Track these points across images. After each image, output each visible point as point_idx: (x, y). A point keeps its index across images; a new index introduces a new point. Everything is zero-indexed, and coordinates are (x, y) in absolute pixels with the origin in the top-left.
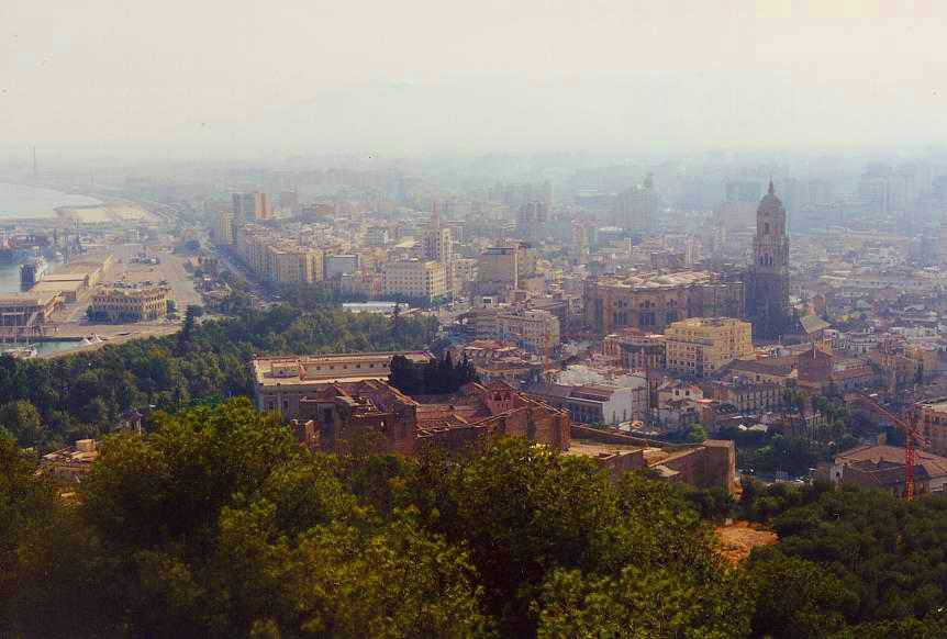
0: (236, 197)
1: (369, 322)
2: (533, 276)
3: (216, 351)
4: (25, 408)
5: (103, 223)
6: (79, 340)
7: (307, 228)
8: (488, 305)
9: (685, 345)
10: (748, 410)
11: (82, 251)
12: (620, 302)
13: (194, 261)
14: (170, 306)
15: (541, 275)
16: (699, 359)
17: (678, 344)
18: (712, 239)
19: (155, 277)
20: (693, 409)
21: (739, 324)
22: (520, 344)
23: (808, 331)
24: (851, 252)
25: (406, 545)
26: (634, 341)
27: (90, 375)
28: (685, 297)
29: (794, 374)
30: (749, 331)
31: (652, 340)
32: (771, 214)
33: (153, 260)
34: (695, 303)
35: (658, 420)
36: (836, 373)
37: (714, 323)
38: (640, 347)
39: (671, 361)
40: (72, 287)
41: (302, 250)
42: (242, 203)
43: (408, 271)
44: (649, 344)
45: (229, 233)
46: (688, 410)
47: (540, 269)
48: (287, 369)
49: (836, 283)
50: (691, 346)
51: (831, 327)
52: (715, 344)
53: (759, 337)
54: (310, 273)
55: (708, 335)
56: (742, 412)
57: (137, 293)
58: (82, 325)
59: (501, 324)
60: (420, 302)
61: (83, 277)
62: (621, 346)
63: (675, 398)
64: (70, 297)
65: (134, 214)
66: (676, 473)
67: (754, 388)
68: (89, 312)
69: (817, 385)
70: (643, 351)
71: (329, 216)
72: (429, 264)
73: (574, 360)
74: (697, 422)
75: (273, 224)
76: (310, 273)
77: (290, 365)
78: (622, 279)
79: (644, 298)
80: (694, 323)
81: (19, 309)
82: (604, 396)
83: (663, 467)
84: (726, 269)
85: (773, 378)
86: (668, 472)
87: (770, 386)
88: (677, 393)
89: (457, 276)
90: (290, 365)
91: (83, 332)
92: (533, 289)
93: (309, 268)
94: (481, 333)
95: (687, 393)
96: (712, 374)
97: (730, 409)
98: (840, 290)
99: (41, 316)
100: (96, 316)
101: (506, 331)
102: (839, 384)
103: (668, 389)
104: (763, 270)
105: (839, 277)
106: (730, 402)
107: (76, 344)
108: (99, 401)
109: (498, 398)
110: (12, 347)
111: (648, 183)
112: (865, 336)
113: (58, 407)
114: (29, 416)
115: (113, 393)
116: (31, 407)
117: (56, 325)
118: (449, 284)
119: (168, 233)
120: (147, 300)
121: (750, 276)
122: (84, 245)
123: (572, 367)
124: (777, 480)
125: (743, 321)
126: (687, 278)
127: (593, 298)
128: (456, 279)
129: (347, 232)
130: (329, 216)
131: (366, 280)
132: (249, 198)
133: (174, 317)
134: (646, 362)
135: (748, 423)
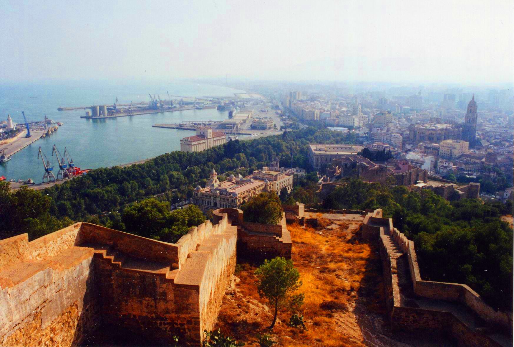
0: (291, 93)
1: (338, 134)
2: (391, 123)
3: (294, 140)
4: (242, 155)
5: (249, 99)
6: (250, 134)
7: (313, 103)
8: (378, 131)
9: (446, 148)
10: (468, 171)
11: (245, 107)
12: (422, 133)
13: (279, 112)
14: (275, 126)
15: (393, 122)
16: (451, 153)
17: (444, 148)
18: (441, 112)
19: (268, 116)
20: (451, 169)
21: (465, 142)
22: (390, 144)
23: (483, 145)
24: (490, 119)
25: (436, 222)
26: (429, 146)
27: (260, 146)
28: (443, 132)
29: (484, 160)
30: (468, 145)
31: (434, 146)
32: (472, 106)
33: (266, 111)
34: (446, 134)
35: (439, 172)
36: (498, 160)
37: (457, 142)
38: (431, 148)
39: (441, 153)
40: (245, 118)
41: (313, 110)
42: (293, 95)
43: (346, 118)
44: (434, 147)
45: (288, 103)
46: (450, 169)
47: (393, 121)
48: (321, 148)
49: (488, 129)
50: (449, 148)
51: (490, 145)
52: (457, 148)
53: (471, 146)
54: (316, 117)
55: (455, 146)
56: (467, 171)
57: (265, 121)
58: (248, 130)
59: (384, 137)
60: (350, 128)
61: (247, 115)
62: (424, 147)
63: (444, 165)
64: (245, 121)
65: (257, 96)
66: (463, 193)
67: (471, 164)
68: (251, 126)
69: (492, 164)
70: (431, 149)
71: (319, 99)
72: (354, 116)
73: (410, 150)
74: (452, 173)
75: (302, 101)
76: (316, 117)
77: (322, 147)
78: (422, 125)
79: (430, 132)
80: (449, 141)
81: (231, 124)
82: (422, 163)
83: (459, 191)
84: (456, 124)
85: (477, 161)
86: (461, 192)
87: (475, 163)
88: (446, 164)
89: (362, 120)
90: (322, 147)
91: (250, 132)
92: (391, 126)
93: (316, 115)
94: (376, 140)
95: (449, 164)
96: (455, 158)
97: (463, 170)
98: (490, 132)
99: (237, 126)
100: (253, 127)
101: (385, 140)
102: (499, 165)
103: (441, 162)
104: (468, 124)
105: (488, 128)
106: (463, 167)
107: (249, 136)
108: (263, 154)
109: (403, 164)
110: (232, 136)
111: (420, 93)
112: (504, 148)
113: (251, 156)
114: (243, 158)
115: (267, 152)
116: (244, 156)
117: (242, 130)
118: (359, 123)
119: (268, 102)
120: (269, 123)
121: (464, 126)
122: (245, 105)
123: (410, 153)
124: (482, 195)
125: (466, 141)
126: (444, 126)
127: (411, 129)
128: (361, 121)
129: (325, 105)
130: (319, 99)
131: (334, 120)
132: (295, 93)
133: (276, 129)
134: (432, 153)
135: (469, 175)
